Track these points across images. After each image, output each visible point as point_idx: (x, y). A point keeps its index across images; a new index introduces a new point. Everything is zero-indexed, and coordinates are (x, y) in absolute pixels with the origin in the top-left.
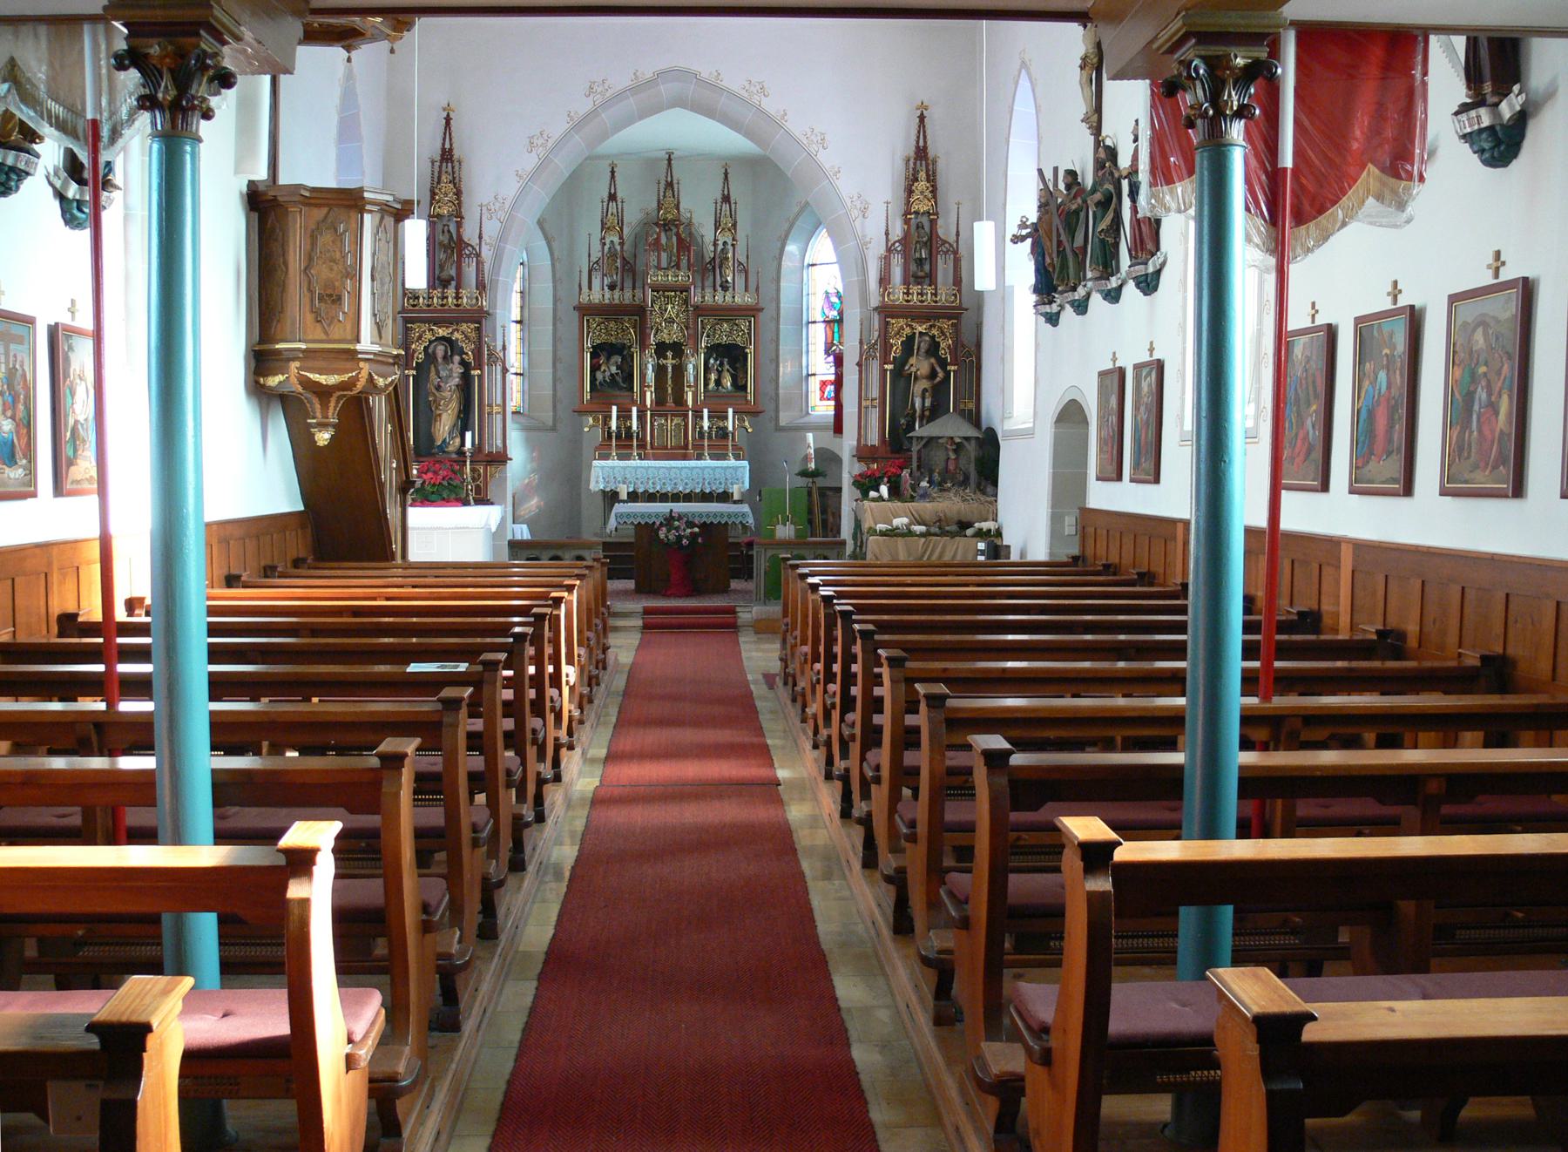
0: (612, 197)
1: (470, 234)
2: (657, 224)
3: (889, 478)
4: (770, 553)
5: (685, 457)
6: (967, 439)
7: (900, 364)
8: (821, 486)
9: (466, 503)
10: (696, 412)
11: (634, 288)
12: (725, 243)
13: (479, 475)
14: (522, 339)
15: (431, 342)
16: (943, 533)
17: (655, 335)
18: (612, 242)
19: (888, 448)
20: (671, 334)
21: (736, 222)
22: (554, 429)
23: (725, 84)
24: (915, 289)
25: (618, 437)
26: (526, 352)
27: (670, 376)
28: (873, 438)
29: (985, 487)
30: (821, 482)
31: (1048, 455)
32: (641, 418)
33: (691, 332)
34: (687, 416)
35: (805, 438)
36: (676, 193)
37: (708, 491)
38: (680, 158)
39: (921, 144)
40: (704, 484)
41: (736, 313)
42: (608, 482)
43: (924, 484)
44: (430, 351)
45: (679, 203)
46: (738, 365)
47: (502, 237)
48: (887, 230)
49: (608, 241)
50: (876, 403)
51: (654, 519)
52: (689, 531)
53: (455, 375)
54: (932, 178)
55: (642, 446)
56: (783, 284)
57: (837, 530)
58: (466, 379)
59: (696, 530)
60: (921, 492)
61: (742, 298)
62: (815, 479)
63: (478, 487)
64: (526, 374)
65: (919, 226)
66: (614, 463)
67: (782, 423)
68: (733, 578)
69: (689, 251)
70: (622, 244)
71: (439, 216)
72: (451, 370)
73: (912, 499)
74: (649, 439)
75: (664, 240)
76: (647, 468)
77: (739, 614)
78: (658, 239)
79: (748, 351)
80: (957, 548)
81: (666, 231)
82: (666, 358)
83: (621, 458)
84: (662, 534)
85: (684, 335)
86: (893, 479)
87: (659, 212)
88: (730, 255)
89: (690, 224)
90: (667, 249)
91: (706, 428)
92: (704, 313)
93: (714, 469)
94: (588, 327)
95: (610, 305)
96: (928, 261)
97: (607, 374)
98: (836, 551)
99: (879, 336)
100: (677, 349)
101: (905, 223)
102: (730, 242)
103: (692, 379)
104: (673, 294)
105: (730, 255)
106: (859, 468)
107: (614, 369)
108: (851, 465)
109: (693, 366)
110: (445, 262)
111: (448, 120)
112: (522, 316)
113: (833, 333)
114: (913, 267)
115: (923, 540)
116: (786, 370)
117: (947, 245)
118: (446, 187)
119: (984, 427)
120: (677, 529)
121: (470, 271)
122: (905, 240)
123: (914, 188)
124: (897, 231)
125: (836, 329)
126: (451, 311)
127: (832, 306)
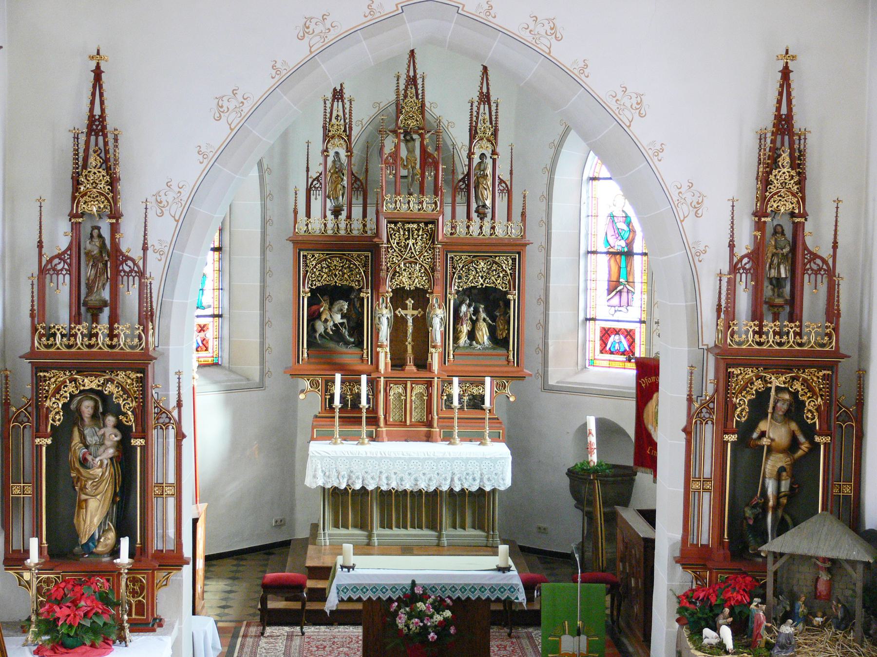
1: (130, 243)
3: (732, 609)
6: (853, 563)
7: (746, 429)
12: (483, 156)
15: (72, 396)
18: (337, 153)
22: (261, 386)
23: (499, 21)
26: (226, 286)
27: (410, 330)
28: (705, 536)
32: (373, 384)
36: (420, 92)
39: (784, 111)
40: (452, 480)
42: (329, 477)
44: (73, 406)
48: (732, 241)
49: (332, 153)
51: (389, 594)
52: (438, 618)
54: (798, 162)
56: (555, 205)
63: (140, 605)
64: (226, 315)
65: (778, 231)
67: (552, 382)
68: (494, 624)
70: (349, 157)
75: (404, 153)
78: (395, 155)
79: (510, 297)
81: (407, 141)
84: (401, 621)
86: (737, 610)
87: (398, 118)
88: (489, 171)
95: (335, 236)
97: (330, 324)
99: (716, 391)
100: (421, 297)
102: (488, 155)
104: (415, 226)
105: (489, 171)
107: (338, 318)
109: (439, 318)
110: (94, 282)
111: (98, 73)
112: (221, 240)
113: (620, 268)
114: (768, 291)
117: (818, 261)
118: (96, 174)
120: (421, 615)
121: (130, 296)
122: (756, 255)
123: (772, 177)
124: (744, 244)
125: (623, 265)
127: (619, 234)
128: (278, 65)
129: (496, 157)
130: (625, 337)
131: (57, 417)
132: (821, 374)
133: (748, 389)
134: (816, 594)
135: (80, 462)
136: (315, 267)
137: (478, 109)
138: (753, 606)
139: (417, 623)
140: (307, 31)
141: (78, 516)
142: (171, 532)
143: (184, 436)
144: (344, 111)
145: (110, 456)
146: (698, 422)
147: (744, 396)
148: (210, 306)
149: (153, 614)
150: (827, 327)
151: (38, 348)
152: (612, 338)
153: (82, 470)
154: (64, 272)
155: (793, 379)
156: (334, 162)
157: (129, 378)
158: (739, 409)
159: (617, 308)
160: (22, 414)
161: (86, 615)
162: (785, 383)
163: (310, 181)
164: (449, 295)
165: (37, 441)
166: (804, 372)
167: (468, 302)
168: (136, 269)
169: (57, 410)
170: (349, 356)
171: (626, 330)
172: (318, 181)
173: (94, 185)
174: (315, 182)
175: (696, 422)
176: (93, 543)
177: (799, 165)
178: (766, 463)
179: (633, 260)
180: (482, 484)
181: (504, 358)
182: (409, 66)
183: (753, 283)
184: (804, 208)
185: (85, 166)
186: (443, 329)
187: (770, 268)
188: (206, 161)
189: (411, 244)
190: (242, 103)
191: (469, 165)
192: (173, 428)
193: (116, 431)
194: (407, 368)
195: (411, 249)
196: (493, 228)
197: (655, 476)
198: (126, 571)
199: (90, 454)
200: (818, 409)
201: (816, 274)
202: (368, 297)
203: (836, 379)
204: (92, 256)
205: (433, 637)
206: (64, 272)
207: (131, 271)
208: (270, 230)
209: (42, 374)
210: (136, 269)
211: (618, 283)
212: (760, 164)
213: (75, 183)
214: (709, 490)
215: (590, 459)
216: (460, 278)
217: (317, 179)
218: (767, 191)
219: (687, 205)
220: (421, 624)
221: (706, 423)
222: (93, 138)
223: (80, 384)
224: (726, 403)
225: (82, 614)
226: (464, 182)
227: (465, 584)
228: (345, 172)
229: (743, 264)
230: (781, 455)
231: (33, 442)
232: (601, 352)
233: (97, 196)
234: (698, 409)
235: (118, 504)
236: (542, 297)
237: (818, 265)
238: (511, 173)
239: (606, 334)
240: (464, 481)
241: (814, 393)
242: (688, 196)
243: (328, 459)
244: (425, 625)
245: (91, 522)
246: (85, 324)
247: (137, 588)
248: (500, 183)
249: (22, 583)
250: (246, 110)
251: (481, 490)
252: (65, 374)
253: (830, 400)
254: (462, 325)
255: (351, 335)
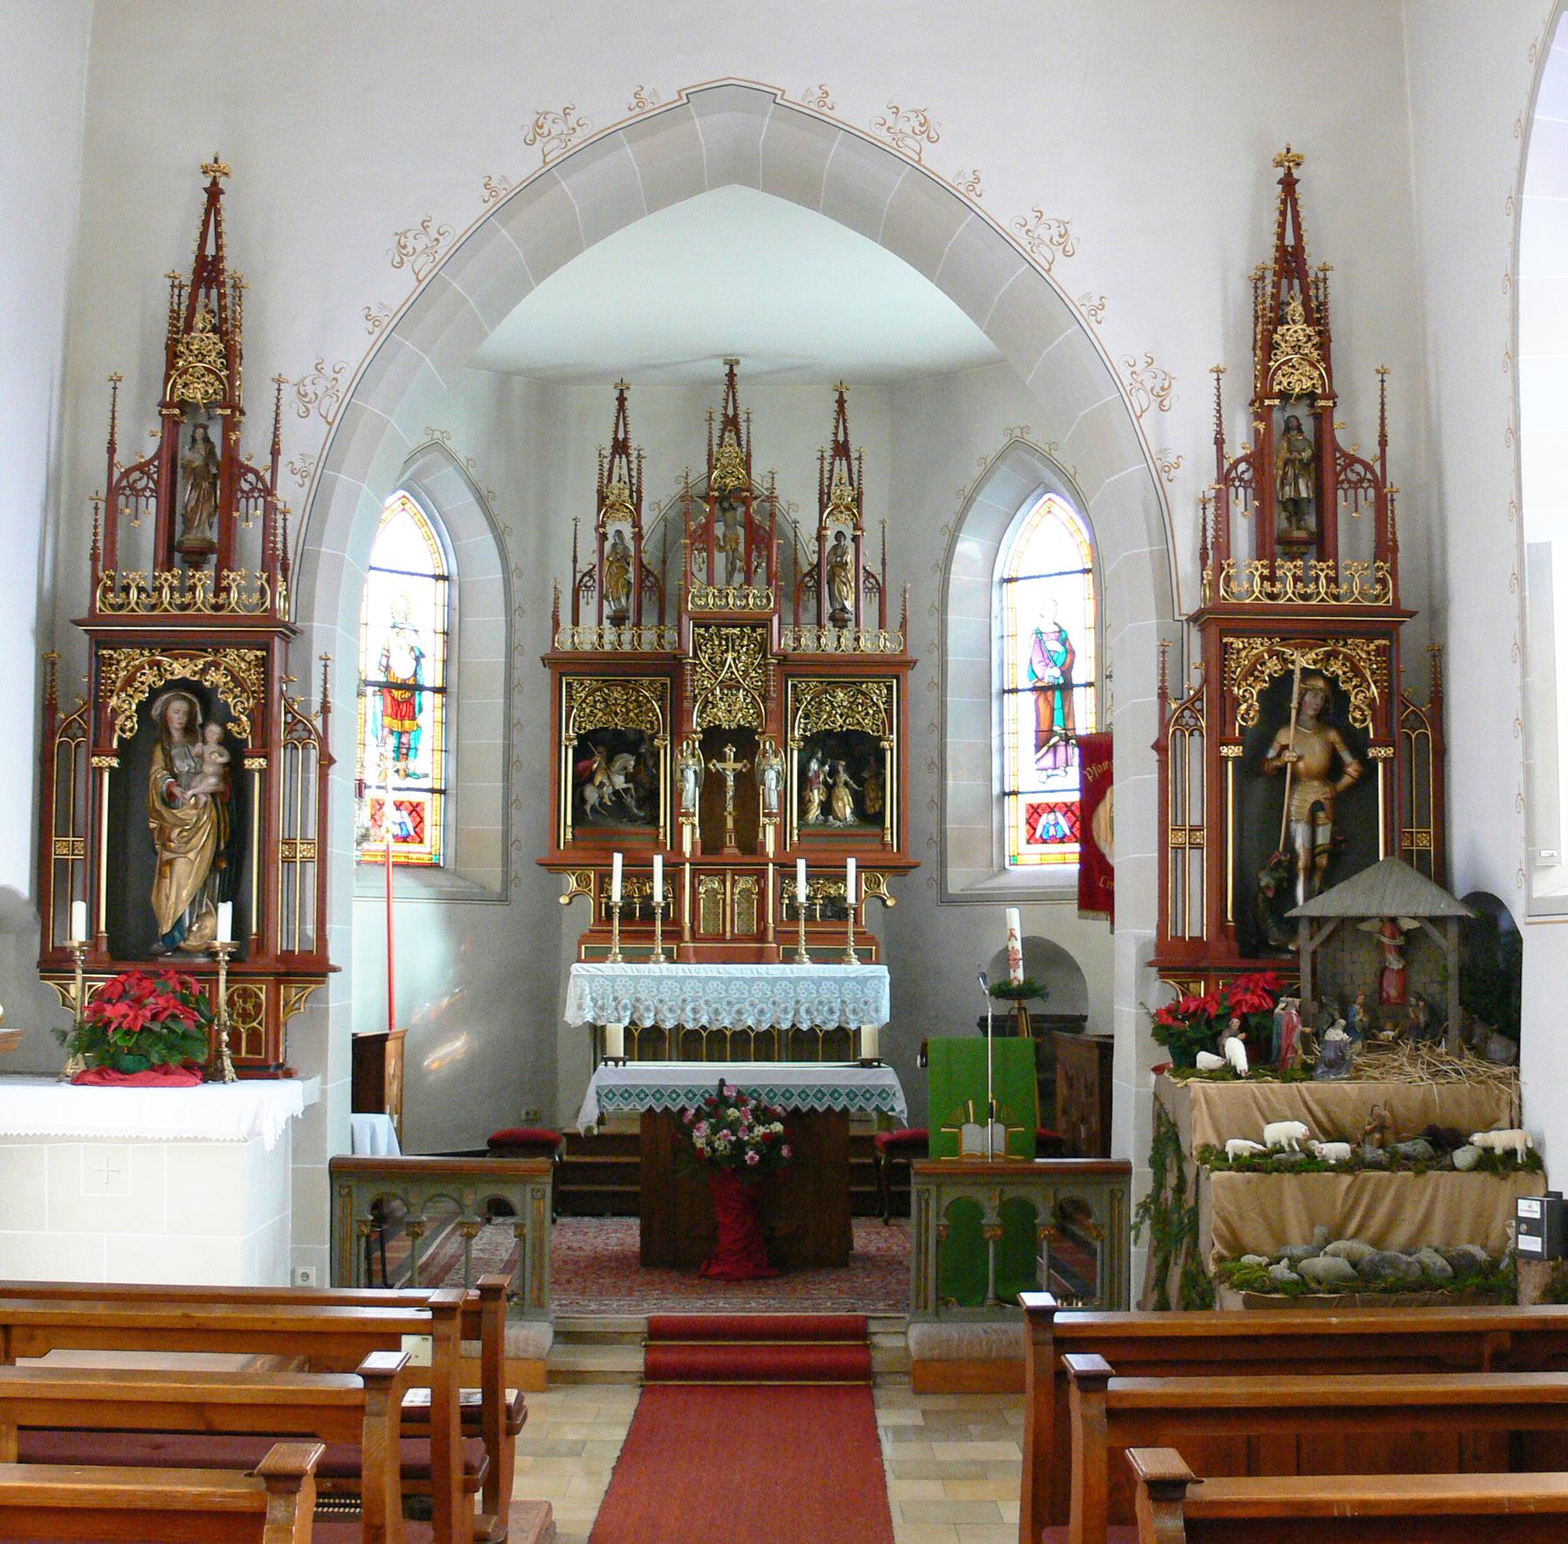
0: (620, 447)
1: (253, 448)
2: (706, 498)
3: (1244, 1019)
4: (949, 1195)
5: (759, 958)
6: (1436, 921)
7: (1259, 741)
8: (1038, 1012)
9: (211, 1073)
10: (782, 865)
11: (661, 621)
12: (839, 535)
13: (258, 1006)
14: (445, 723)
16: (1397, 1162)
17: (702, 712)
18: (619, 532)
19: (1235, 945)
20: (732, 712)
21: (860, 494)
22: (503, 899)
24: (1286, 569)
25: (627, 914)
26: (452, 747)
27: (730, 793)
28: (1195, 923)
29: (1486, 1039)
30: (1035, 1007)
31: (334, 900)
32: (672, 877)
33: (772, 705)
34: (762, 875)
35: (1003, 920)
37: (805, 1027)
38: (753, 377)
39: (1290, 240)
40: (797, 1012)
41: (867, 671)
42: (602, 1008)
43: (1336, 1034)
44: (156, 711)
45: (749, 455)
46: (865, 775)
47: (331, 456)
48: (1219, 433)
49: (610, 530)
50: (1201, 837)
51: (682, 1102)
52: (760, 1130)
53: (209, 769)
54: (1317, 316)
55: (673, 934)
56: (952, 617)
57: (1102, 1141)
58: (235, 776)
59: (778, 1127)
60: (1330, 1054)
61: (873, 642)
62: (1025, 1003)
63: (254, 1035)
64: (452, 791)
65: (1292, 427)
66: (616, 968)
67: (954, 887)
68: (858, 1214)
69: (769, 548)
70: (638, 537)
71: (183, 405)
72: (201, 756)
73: (1308, 1072)
74: (687, 919)
75: (719, 529)
76: (681, 981)
77: (876, 1339)
78: (707, 528)
79: (885, 744)
80: (1432, 1202)
82: (722, 758)
83: (630, 958)
84: (700, 1137)
85: (759, 715)
86: (1253, 1021)
87: (710, 473)
88: (850, 558)
89: (771, 498)
90: (726, 545)
91: (802, 898)
92: (803, 671)
93: (818, 982)
94: (570, 697)
95: (614, 654)
96: (1312, 508)
97: (607, 790)
98: (1106, 1190)
99: (1205, 680)
100: (745, 741)
101: (1258, 417)
102: (849, 533)
103: (774, 800)
104: (737, 631)
105: (850, 558)
106: (1162, 994)
107: (620, 782)
108: (1142, 982)
111: (214, 193)
112: (445, 677)
113: (1053, 710)
114: (1281, 521)
115: (1346, 1180)
116: (961, 786)
117: (1358, 468)
118: (203, 340)
119: (1461, 888)
120: (733, 1126)
121: (250, 530)
122: (1259, 458)
123: (1276, 337)
124: (1240, 442)
125: (1058, 704)
126: (199, 619)
127: (1049, 658)
128: (493, 183)
129: (859, 533)
130: (1065, 814)
131: (129, 724)
132: (1372, 646)
133: (1256, 673)
134: (1381, 997)
135: (163, 799)
136: (584, 701)
137: (832, 464)
138: (1277, 1010)
139: (725, 1136)
140: (540, 131)
141: (159, 891)
142: (311, 929)
143: (332, 761)
144: (630, 470)
145: (210, 789)
146: (1178, 733)
147: (1250, 685)
148: (426, 776)
149: (277, 1057)
150: (1379, 569)
151: (101, 610)
152: (1046, 819)
153: (165, 812)
154: (148, 493)
155: (1328, 655)
156: (614, 545)
157: (243, 660)
158: (1244, 707)
159: (1050, 772)
160: (75, 725)
161: (154, 1017)
162: (1315, 662)
163: (579, 576)
164: (790, 742)
165: (95, 760)
166: (1345, 644)
167: (820, 755)
168: (260, 486)
169: (128, 713)
170: (636, 835)
171: (1065, 804)
172: (591, 577)
173: (200, 358)
174: (587, 578)
175: (1174, 732)
176: (182, 934)
177: (1319, 319)
178: (1291, 797)
179: (1072, 695)
180: (843, 1018)
181: (877, 840)
182: (727, 401)
183: (1257, 503)
184: (1330, 387)
185: (189, 328)
186: (781, 788)
187: (1283, 484)
188: (377, 331)
189: (730, 660)
190: (437, 240)
191: (820, 553)
192: (314, 747)
193: (222, 749)
194: (726, 851)
195: (730, 666)
196: (857, 639)
197: (1112, 923)
198: (227, 958)
199: (179, 785)
200: (1371, 703)
201: (1356, 489)
202: (666, 747)
203: (1398, 652)
204: (194, 469)
205: (752, 1158)
206: (148, 493)
207: (252, 490)
208: (517, 660)
209: (105, 652)
210: (260, 486)
211: (1051, 733)
212: (1256, 318)
213: (171, 355)
214: (1199, 847)
215: (1012, 975)
216: (807, 716)
217: (589, 573)
218: (1270, 359)
219: (1146, 393)
220: (734, 1138)
221: (1191, 734)
222: (202, 292)
223: (166, 670)
224: (1222, 696)
225: (149, 1015)
226: (812, 577)
227: (807, 1086)
228: (631, 561)
229: (1239, 471)
230: (1316, 783)
231: (88, 763)
232: (1028, 842)
233: (203, 375)
234: (1176, 710)
235: (223, 873)
236: (936, 760)
237: (251, 483)
238: (884, 563)
239: (1035, 811)
240: (815, 1014)
241: (1364, 679)
242: (1147, 378)
243: (601, 980)
244: (739, 1139)
245: (178, 896)
246: (177, 571)
247: (249, 1006)
248: (866, 579)
249: (67, 1002)
250: (442, 251)
251: (840, 1029)
252: (142, 655)
253: (1390, 687)
254: (812, 791)
255: (639, 808)
